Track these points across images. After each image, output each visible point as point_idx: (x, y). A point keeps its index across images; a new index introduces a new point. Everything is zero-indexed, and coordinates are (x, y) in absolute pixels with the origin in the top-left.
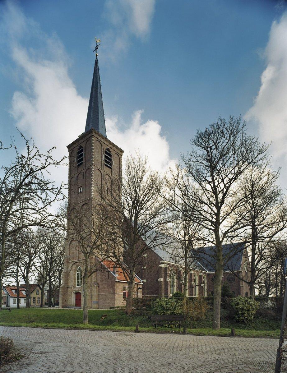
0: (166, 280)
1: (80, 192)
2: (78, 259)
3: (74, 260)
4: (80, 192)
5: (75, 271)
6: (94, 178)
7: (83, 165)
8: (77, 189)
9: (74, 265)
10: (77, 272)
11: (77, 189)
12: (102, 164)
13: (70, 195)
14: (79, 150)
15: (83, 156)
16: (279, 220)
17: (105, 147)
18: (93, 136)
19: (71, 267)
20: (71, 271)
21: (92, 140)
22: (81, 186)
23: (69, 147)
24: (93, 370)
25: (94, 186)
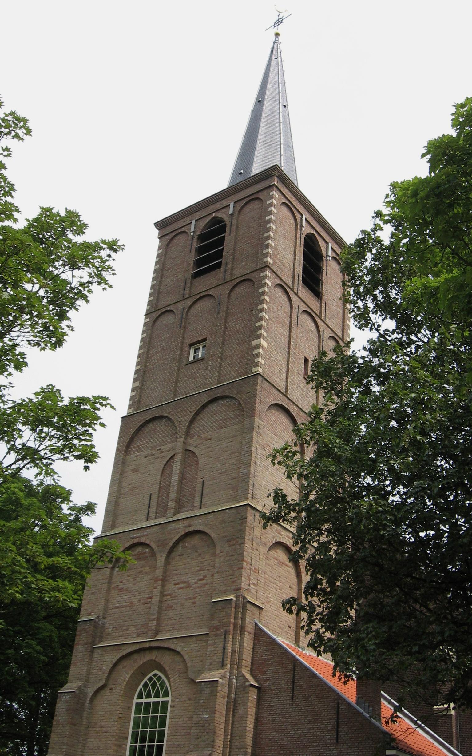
0: (402, 485)
1: (191, 359)
2: (157, 633)
3: (126, 636)
4: (191, 359)
5: (128, 695)
6: (269, 309)
7: (222, 269)
8: (182, 349)
9: (125, 663)
10: (140, 696)
11: (182, 349)
12: (296, 275)
13: (144, 372)
14: (202, 230)
15: (224, 232)
16: (159, 343)
17: (307, 230)
18: (275, 188)
19: (106, 668)
20: (106, 693)
21: (272, 197)
22: (205, 340)
23: (161, 225)
24: (200, 722)
25: (265, 334)
